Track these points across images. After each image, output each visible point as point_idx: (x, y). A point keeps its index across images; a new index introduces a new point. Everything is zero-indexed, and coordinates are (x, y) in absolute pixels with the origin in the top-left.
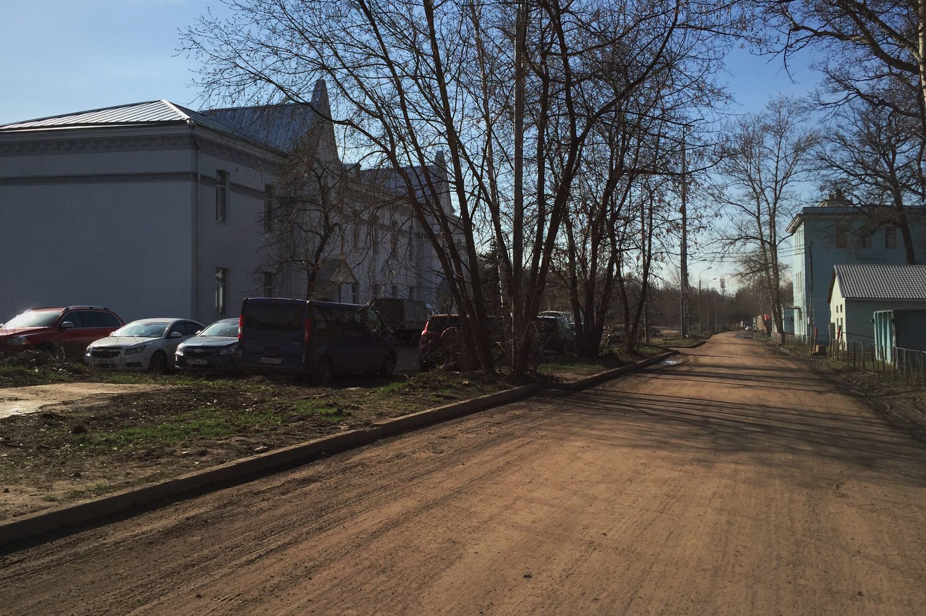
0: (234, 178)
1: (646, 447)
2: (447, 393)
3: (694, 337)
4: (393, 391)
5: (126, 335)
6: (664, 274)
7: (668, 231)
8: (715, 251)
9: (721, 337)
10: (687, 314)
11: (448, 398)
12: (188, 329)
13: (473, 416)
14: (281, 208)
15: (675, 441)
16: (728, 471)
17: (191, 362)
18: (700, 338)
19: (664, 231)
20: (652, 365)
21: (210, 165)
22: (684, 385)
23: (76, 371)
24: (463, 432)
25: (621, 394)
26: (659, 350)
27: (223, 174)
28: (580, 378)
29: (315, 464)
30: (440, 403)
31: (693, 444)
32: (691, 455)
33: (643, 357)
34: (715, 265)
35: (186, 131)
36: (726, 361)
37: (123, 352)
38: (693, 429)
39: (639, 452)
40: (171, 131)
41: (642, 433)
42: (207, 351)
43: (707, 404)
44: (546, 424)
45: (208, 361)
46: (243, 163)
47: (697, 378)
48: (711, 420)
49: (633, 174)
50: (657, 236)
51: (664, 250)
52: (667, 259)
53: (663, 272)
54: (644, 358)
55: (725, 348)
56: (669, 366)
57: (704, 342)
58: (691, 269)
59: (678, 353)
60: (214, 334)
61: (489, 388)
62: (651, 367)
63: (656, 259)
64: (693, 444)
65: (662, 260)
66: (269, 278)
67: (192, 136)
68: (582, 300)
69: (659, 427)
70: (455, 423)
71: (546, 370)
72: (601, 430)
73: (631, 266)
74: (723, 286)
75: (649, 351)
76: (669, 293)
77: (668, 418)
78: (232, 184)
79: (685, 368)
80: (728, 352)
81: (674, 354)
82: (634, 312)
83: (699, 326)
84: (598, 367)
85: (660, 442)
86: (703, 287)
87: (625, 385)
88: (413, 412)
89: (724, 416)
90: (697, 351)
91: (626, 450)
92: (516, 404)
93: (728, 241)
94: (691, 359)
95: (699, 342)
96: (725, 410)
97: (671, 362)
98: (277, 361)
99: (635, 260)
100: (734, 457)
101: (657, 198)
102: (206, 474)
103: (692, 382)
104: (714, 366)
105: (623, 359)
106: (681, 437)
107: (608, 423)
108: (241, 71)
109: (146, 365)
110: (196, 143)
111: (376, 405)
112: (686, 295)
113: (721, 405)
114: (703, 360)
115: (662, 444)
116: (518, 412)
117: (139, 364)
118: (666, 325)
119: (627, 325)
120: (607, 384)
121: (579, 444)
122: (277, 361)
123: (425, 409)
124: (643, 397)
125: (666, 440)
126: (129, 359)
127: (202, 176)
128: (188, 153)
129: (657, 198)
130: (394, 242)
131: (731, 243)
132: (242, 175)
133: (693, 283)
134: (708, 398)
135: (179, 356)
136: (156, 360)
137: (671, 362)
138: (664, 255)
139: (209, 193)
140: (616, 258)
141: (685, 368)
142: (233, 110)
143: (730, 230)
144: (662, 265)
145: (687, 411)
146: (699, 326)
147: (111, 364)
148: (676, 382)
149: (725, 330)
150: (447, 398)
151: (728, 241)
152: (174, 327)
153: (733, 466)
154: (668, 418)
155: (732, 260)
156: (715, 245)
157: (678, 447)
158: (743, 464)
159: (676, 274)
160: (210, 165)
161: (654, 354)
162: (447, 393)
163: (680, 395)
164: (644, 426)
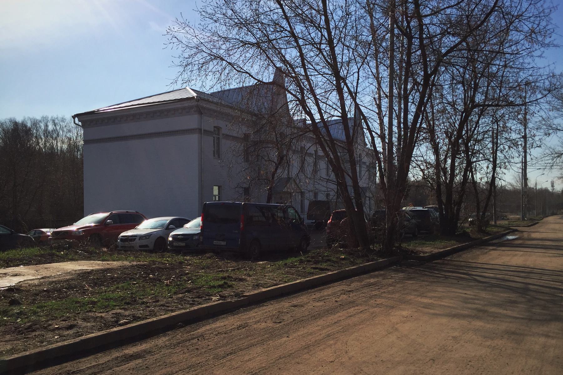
0: (224, 131)
1: (464, 317)
2: (324, 266)
3: (531, 219)
4: (286, 264)
5: (147, 226)
6: (508, 178)
7: (509, 147)
8: (547, 162)
9: (551, 219)
10: (525, 205)
11: (322, 270)
12: (179, 223)
13: (336, 284)
14: (252, 149)
15: (493, 310)
16: (537, 348)
17: (175, 244)
18: (535, 220)
19: (507, 147)
20: (496, 240)
21: (210, 123)
22: (516, 255)
23: (91, 253)
24: (309, 301)
25: (463, 264)
26: (503, 229)
27: (218, 128)
28: (436, 251)
29: (263, 306)
30: (312, 274)
31: (509, 313)
32: (503, 326)
33: (488, 234)
34: (546, 172)
35: (194, 103)
36: (552, 236)
37: (138, 238)
38: (513, 296)
39: (456, 323)
40: (186, 104)
41: (466, 301)
42: (186, 237)
43: (528, 271)
44: (389, 292)
45: (187, 244)
46: (245, 124)
47: (529, 250)
48: (531, 287)
49: (483, 109)
50: (502, 151)
51: (506, 161)
52: (509, 167)
53: (505, 176)
54: (490, 234)
55: (552, 226)
56: (508, 240)
57: (538, 223)
58: (529, 175)
59: (517, 230)
60: (193, 226)
61: (359, 261)
62: (494, 241)
63: (500, 168)
64: (509, 313)
65: (505, 168)
66: (247, 191)
67: (197, 106)
68: (444, 199)
69: (483, 294)
70: (316, 291)
71: (411, 246)
72: (431, 298)
73: (481, 175)
74: (553, 186)
75: (495, 230)
76: (514, 193)
77: (493, 286)
78: (223, 134)
79: (520, 242)
80: (554, 229)
81: (513, 232)
82: (482, 205)
83: (535, 212)
84: (453, 242)
85: (480, 310)
86: (539, 187)
87: (467, 256)
88: (286, 282)
89: (542, 283)
90: (532, 229)
91: (444, 320)
92: (377, 273)
93: (556, 155)
94: (525, 235)
95: (533, 223)
96: (545, 277)
97: (510, 237)
98: (223, 243)
99: (485, 168)
100: (544, 329)
101: (501, 125)
102: (140, 325)
103: (522, 253)
104: (542, 239)
105: (474, 236)
106: (499, 305)
107: (440, 290)
108: (205, 55)
109: (151, 247)
110: (200, 111)
111: (267, 275)
112: (525, 192)
113: (542, 272)
114: (534, 235)
115: (481, 314)
116: (372, 280)
117: (146, 246)
118: (512, 212)
119: (478, 212)
120: (455, 255)
121: (405, 313)
122: (223, 243)
123: (298, 279)
124: (479, 266)
125: (486, 308)
126: (144, 242)
127: (204, 130)
128: (196, 117)
129: (501, 125)
130: (303, 162)
131: (558, 156)
132: (226, 127)
133: (531, 184)
134: (532, 266)
135: (170, 241)
136: (157, 243)
137: (510, 237)
138: (507, 164)
139: (209, 140)
140: (470, 167)
141: (520, 242)
142: (229, 90)
143: (558, 148)
144: (505, 171)
145: (512, 278)
146: (535, 212)
147: (132, 246)
148: (510, 253)
149: (553, 214)
150: (322, 270)
151: (556, 155)
152: (171, 222)
153: (542, 340)
154: (493, 286)
155: (558, 167)
156: (547, 158)
157: (495, 316)
158: (553, 338)
159: (518, 179)
160: (210, 123)
161: (498, 232)
162: (324, 266)
163: (509, 264)
164: (470, 293)
